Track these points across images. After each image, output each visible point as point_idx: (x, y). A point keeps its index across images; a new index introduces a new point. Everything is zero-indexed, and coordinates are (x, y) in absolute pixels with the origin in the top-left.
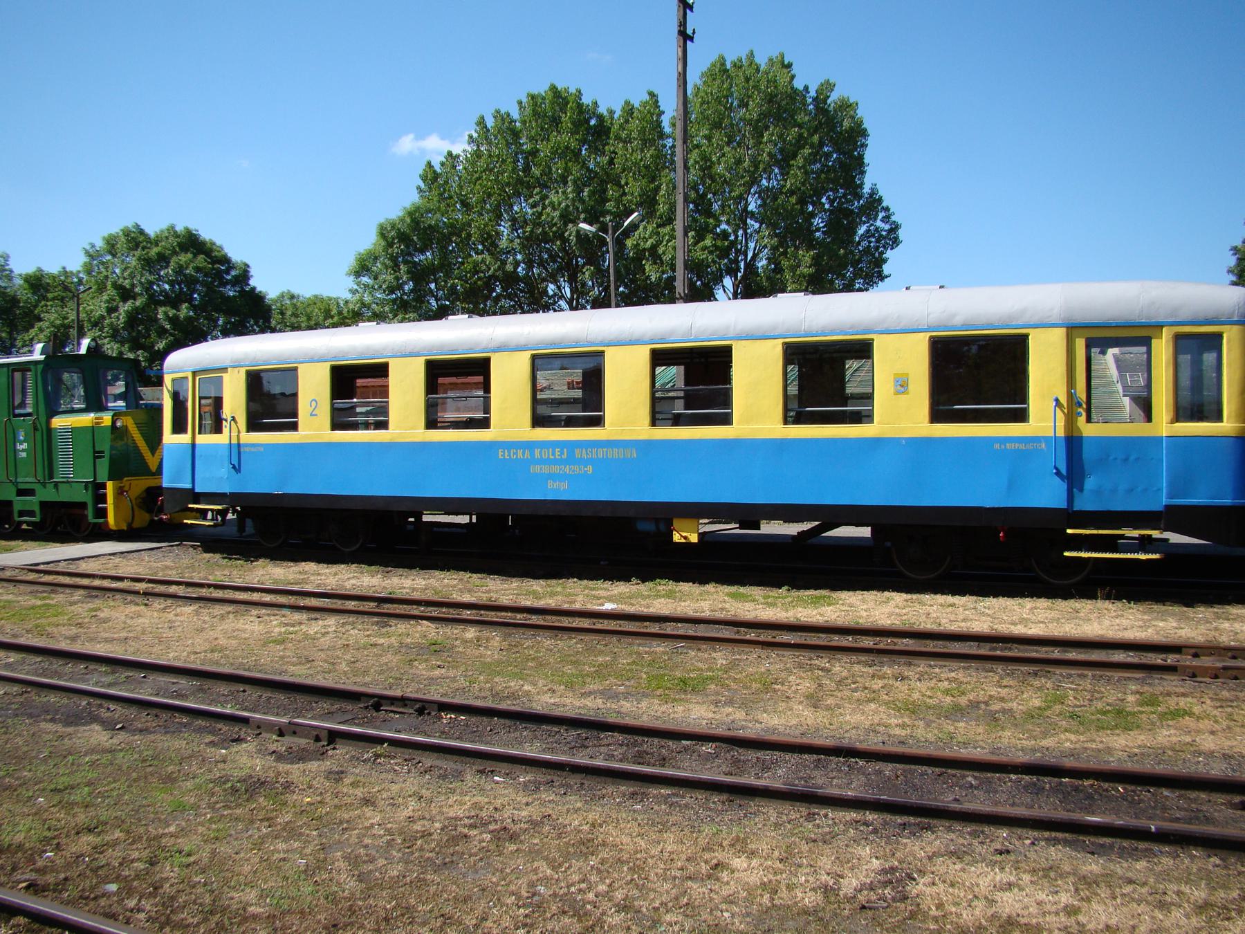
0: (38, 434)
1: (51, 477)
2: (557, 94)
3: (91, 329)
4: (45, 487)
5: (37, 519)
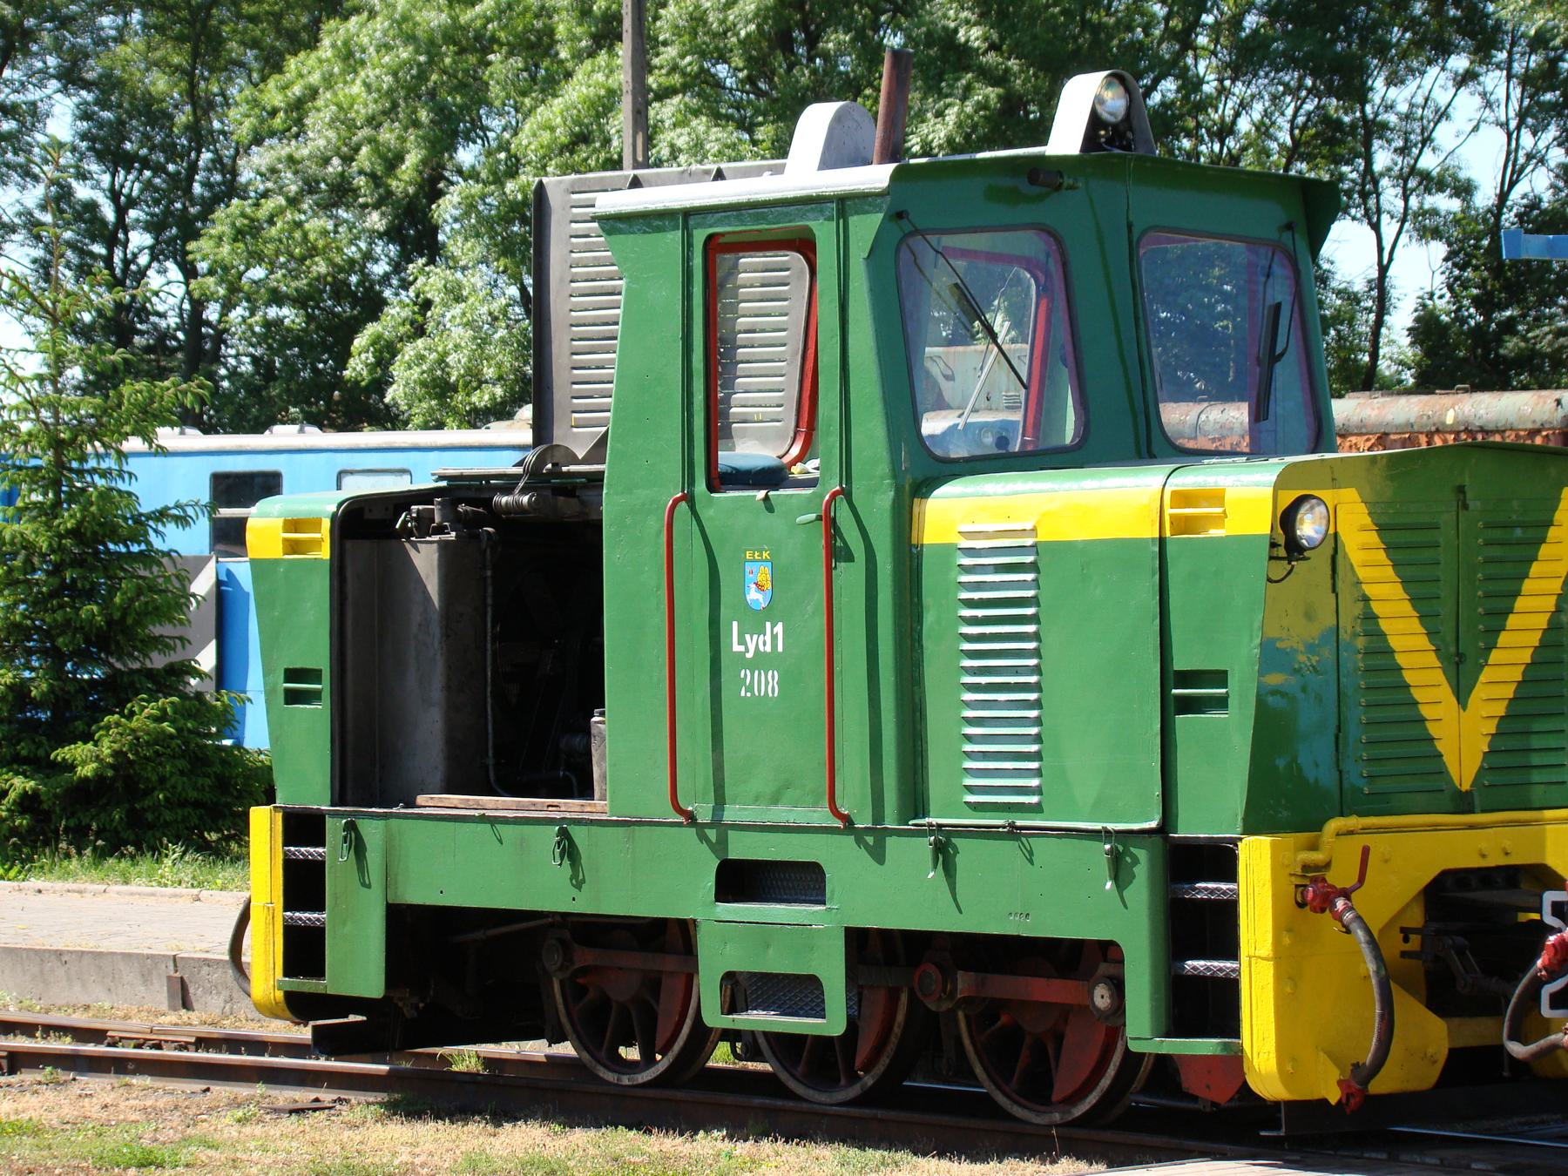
0: (850, 576)
1: (915, 801)
3: (592, 54)
4: (878, 854)
5: (832, 1023)
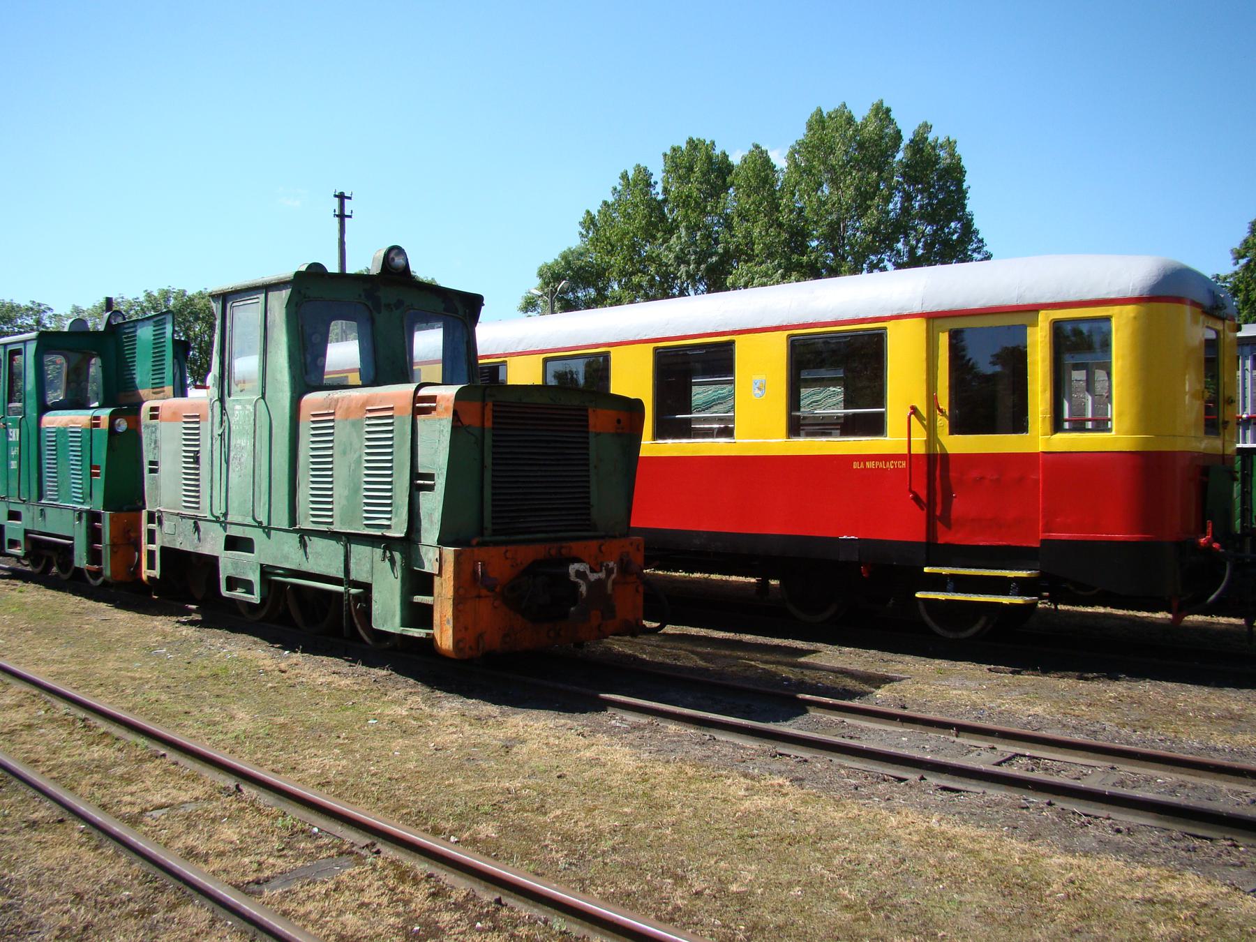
2: (693, 145)
4: (269, 536)
